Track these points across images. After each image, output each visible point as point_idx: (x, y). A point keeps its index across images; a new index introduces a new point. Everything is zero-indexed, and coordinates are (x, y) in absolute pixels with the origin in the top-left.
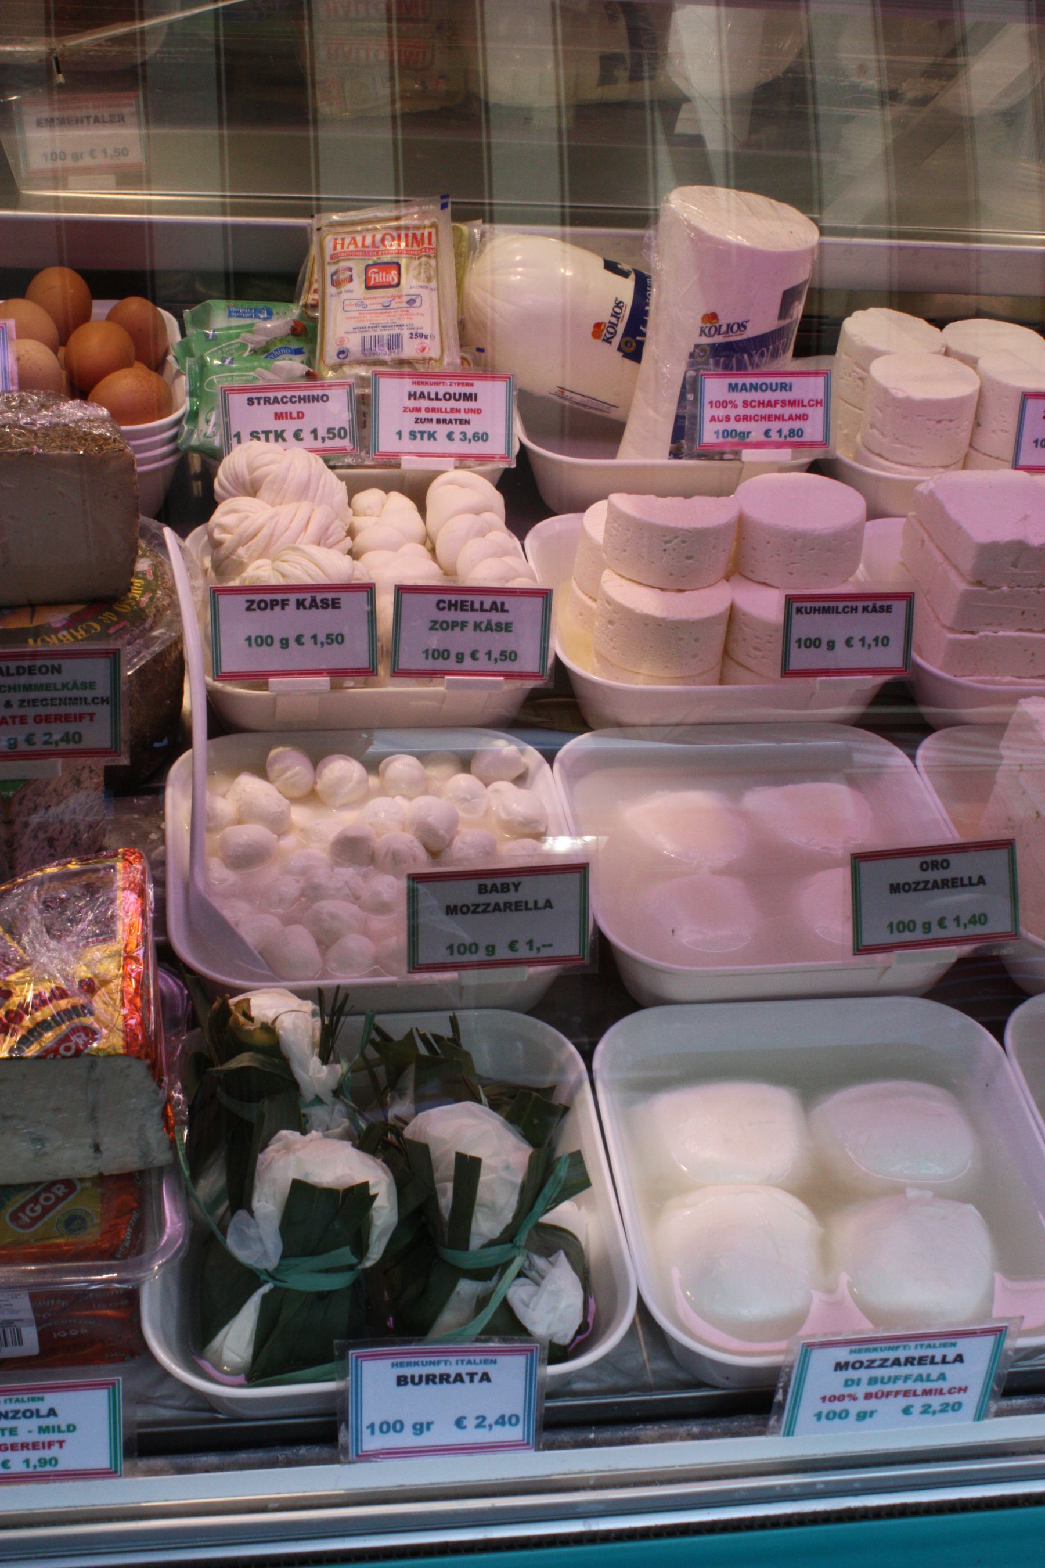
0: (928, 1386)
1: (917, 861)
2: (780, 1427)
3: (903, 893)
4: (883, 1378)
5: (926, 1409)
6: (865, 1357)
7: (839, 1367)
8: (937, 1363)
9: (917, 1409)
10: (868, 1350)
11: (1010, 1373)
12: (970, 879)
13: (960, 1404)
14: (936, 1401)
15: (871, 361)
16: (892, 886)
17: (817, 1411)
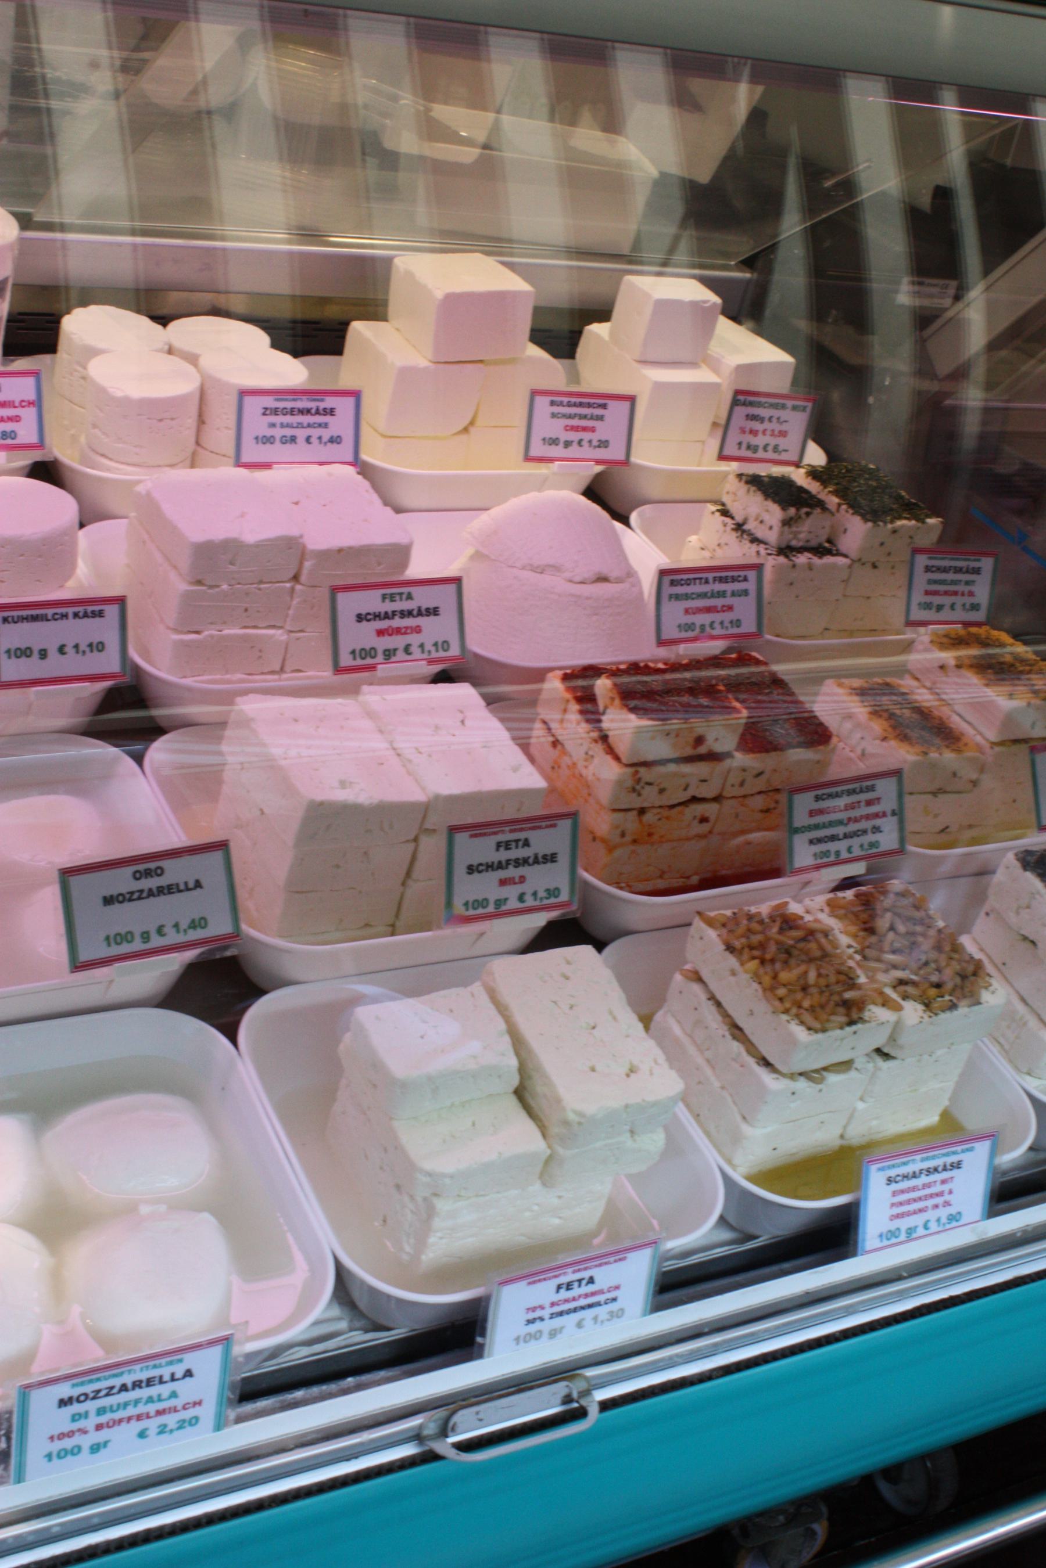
0: (161, 1406)
1: (129, 870)
2: (9, 1476)
3: (117, 905)
4: (111, 1406)
5: (162, 1430)
6: (89, 1389)
7: (63, 1403)
8: (166, 1382)
9: (153, 1431)
10: (91, 1381)
11: (244, 1379)
12: (186, 883)
13: (197, 1418)
14: (171, 1420)
15: (89, 359)
16: (105, 898)
17: (46, 1452)
